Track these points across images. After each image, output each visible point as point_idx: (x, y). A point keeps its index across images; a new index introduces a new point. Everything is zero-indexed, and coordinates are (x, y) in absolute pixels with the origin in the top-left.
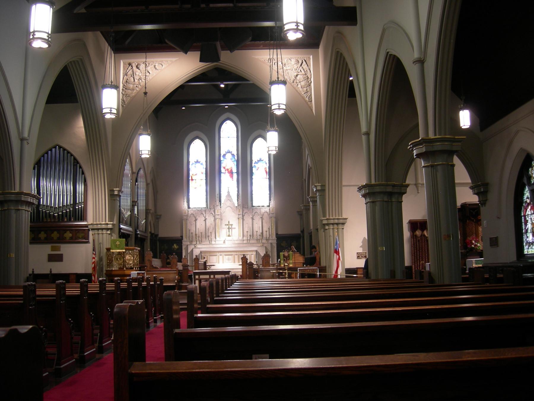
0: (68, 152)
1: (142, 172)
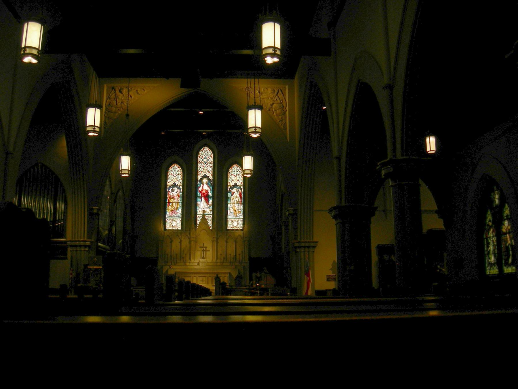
1: (120, 193)
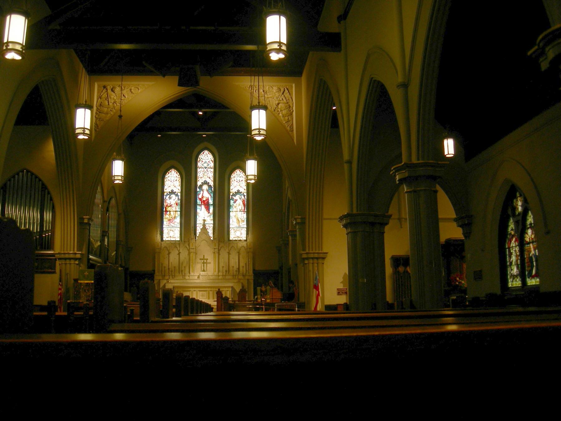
0: (36, 177)
1: (113, 201)
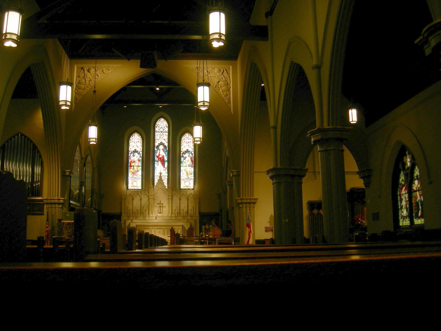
0: (29, 139)
1: (89, 158)
